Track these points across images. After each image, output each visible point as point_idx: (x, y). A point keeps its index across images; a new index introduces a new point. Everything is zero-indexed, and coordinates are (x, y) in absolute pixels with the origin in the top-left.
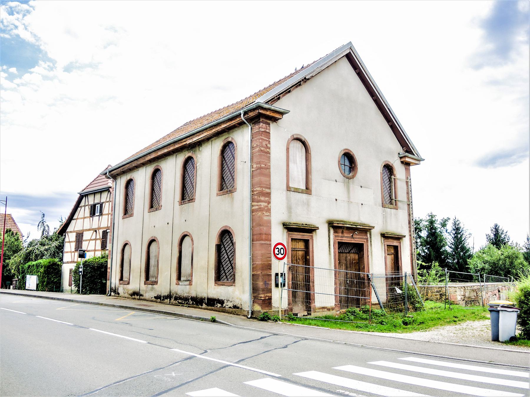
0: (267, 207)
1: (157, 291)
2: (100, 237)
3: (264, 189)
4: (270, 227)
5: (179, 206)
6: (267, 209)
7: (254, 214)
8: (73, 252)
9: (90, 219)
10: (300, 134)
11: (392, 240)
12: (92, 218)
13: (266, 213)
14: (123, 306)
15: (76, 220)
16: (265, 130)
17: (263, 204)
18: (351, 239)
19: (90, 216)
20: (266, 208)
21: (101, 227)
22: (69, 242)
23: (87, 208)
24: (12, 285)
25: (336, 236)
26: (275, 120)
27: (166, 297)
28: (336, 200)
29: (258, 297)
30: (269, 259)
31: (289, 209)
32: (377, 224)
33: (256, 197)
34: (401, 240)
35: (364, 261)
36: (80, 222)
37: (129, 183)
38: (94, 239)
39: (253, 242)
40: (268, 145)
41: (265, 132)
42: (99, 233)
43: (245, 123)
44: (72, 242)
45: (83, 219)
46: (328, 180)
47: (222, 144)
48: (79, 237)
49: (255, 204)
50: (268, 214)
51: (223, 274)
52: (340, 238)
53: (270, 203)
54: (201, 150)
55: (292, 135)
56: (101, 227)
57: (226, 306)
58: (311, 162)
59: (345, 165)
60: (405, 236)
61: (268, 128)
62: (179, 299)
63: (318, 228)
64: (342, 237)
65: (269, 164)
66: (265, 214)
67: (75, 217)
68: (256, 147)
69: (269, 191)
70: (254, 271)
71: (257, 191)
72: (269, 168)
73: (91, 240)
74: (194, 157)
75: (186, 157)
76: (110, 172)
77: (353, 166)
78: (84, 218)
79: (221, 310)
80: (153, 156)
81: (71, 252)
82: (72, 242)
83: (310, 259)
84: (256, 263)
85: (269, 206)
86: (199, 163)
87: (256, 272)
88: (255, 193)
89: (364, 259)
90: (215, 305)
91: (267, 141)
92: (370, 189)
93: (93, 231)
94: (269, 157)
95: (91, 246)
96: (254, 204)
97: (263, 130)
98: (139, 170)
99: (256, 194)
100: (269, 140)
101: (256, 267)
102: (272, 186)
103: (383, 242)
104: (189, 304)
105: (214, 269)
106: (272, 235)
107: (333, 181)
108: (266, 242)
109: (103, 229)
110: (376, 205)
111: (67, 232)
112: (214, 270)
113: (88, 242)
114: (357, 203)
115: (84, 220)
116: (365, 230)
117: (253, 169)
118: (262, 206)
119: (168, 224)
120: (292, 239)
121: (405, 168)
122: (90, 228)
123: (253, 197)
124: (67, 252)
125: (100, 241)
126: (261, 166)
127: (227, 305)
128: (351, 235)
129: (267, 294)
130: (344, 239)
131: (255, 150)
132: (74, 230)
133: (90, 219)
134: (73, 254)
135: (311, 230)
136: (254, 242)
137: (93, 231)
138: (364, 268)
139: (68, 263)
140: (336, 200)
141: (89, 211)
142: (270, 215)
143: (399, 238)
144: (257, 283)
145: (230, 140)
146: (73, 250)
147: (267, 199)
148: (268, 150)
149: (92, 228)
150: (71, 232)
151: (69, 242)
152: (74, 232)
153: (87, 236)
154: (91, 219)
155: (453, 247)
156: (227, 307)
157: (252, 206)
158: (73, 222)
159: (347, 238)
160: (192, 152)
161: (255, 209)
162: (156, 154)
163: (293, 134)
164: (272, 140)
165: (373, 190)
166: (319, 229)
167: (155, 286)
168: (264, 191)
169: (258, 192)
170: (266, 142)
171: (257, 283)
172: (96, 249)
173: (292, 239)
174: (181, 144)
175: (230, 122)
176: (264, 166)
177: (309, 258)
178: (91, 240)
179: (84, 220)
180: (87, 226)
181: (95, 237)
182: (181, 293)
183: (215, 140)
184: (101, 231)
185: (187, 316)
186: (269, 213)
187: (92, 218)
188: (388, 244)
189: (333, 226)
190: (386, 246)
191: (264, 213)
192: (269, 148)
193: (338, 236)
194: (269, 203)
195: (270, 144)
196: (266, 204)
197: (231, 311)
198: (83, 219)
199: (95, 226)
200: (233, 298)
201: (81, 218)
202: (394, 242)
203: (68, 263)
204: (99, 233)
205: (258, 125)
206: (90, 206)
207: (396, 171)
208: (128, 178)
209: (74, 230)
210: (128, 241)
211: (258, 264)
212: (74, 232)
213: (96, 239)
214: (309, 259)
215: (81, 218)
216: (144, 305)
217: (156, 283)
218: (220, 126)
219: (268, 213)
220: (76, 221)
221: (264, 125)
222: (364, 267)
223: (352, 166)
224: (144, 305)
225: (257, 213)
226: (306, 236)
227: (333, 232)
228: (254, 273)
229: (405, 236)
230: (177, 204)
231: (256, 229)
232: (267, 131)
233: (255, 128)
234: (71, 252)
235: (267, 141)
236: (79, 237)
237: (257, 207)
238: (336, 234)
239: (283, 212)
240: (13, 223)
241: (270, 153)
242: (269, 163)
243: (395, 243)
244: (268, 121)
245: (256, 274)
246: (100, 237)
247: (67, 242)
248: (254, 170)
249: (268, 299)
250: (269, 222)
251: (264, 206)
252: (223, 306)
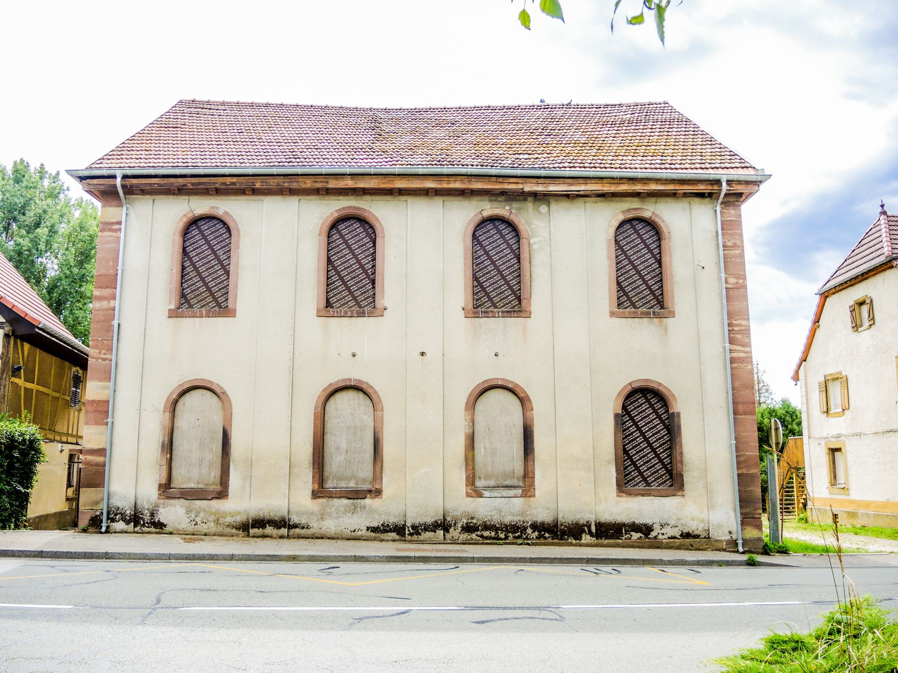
1: (380, 514)
7: (735, 365)
14: (525, 558)
27: (434, 527)
29: (756, 514)
39: (736, 416)
43: (117, 193)
47: (621, 217)
51: (633, 473)
57: (660, 535)
62: (483, 530)
70: (742, 468)
71: (740, 325)
76: (125, 177)
79: (646, 545)
80: (350, 183)
87: (748, 470)
90: (623, 536)
101: (745, 462)
104: (527, 538)
105: (614, 464)
123: (732, 335)
127: (663, 534)
131: (729, 252)
136: (740, 417)
144: (752, 488)
156: (660, 537)
161: (739, 358)
162: (383, 183)
171: (752, 488)
174: (495, 185)
175: (677, 185)
182: (492, 516)
183: (595, 202)
185: (669, 561)
197: (678, 544)
200: (679, 519)
205: (734, 209)
211: (748, 456)
216: (458, 551)
218: (644, 183)
224: (458, 551)
225: (744, 365)
228: (740, 472)
231: (743, 393)
233: (726, 213)
240: (648, 228)
245: (747, 474)
248: (731, 288)
252: (650, 536)
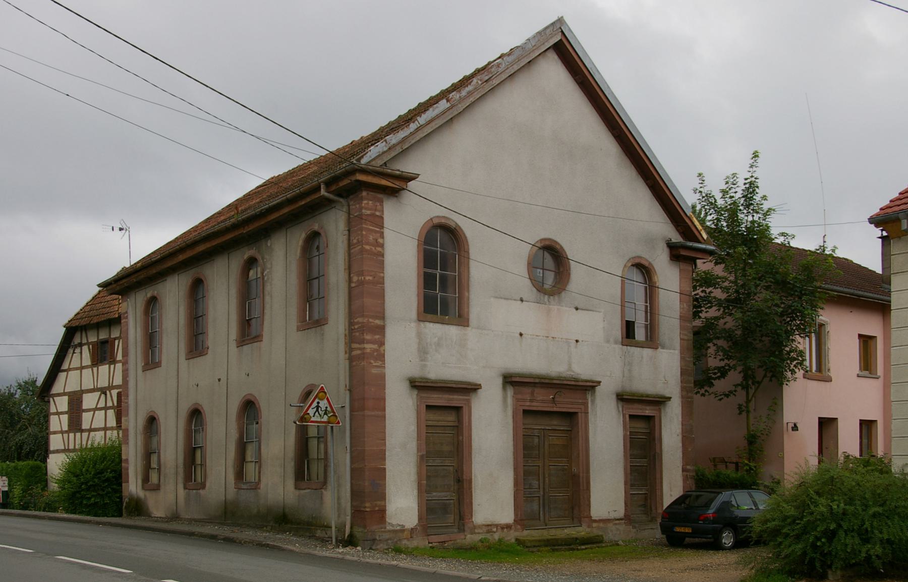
0: (377, 350)
2: (113, 404)
3: (371, 320)
4: (382, 387)
5: (236, 349)
6: (377, 355)
8: (66, 432)
9: (92, 370)
10: (446, 216)
11: (640, 406)
12: (96, 368)
13: (375, 363)
15: (66, 373)
16: (373, 212)
17: (369, 347)
18: (551, 405)
19: (93, 365)
20: (375, 354)
21: (114, 385)
22: (58, 413)
23: (85, 348)
24: (362, 549)
25: (518, 400)
26: (394, 192)
28: (521, 335)
30: (383, 441)
31: (423, 352)
32: (610, 377)
33: (357, 334)
34: (662, 407)
35: (578, 444)
36: (74, 375)
37: (153, 301)
38: (103, 407)
40: (380, 240)
41: (373, 215)
42: (111, 397)
44: (62, 413)
45: (79, 371)
46: (505, 299)
48: (75, 400)
49: (356, 347)
50: (379, 363)
52: (528, 404)
53: (384, 344)
54: (269, 245)
55: (429, 218)
56: (114, 385)
58: (469, 268)
59: (543, 269)
60: (670, 398)
61: (379, 207)
63: (480, 385)
64: (531, 401)
65: (382, 275)
66: (374, 364)
67: (65, 366)
68: (356, 243)
69: (382, 324)
72: (381, 282)
73: (96, 409)
74: (259, 257)
75: (246, 257)
77: (561, 270)
78: (82, 368)
81: (62, 432)
82: (62, 413)
83: (464, 440)
84: (358, 448)
85: (382, 349)
86: (268, 270)
88: (356, 327)
89: (579, 441)
91: (376, 232)
92: (596, 311)
93: (99, 393)
94: (382, 262)
95: (99, 419)
96: (354, 346)
97: (369, 212)
98: (167, 281)
99: (358, 328)
100: (382, 230)
102: (389, 312)
103: (621, 409)
106: (386, 400)
107: (515, 300)
108: (376, 413)
109: (117, 389)
110: (608, 341)
111: (52, 394)
112: (207, 465)
113: (92, 412)
114: (566, 339)
115: (81, 372)
116: (587, 388)
117: (353, 285)
118: (368, 351)
119: (219, 380)
120: (427, 406)
121: (680, 269)
122: (94, 387)
124: (55, 433)
125: (114, 411)
126: (364, 278)
128: (551, 397)
129: (376, 502)
130: (534, 404)
132: (64, 390)
133: (92, 370)
134: (66, 435)
135: (470, 389)
136: (356, 413)
137: (99, 393)
138: (579, 457)
139: (57, 451)
140: (521, 335)
141: (90, 353)
142: (383, 365)
143: (660, 401)
145: (316, 227)
146: (65, 428)
147: (377, 337)
148: (379, 249)
149: (97, 386)
150: (59, 395)
151: (58, 413)
152: (64, 394)
153: (89, 401)
154: (95, 369)
155: (89, 446)
157: (351, 350)
158: (62, 376)
159: (542, 400)
160: (254, 249)
163: (432, 217)
164: (387, 232)
165: (602, 313)
166: (481, 388)
167: (201, 491)
168: (372, 324)
169: (360, 325)
170: (374, 234)
172: (107, 426)
173: (427, 406)
176: (371, 278)
177: (463, 438)
178: (96, 409)
179: (81, 372)
180: (88, 384)
181: (104, 403)
184: (115, 393)
186: (382, 361)
187: (96, 368)
188: (631, 414)
189: (511, 381)
190: (627, 416)
191: (372, 361)
192: (382, 246)
193: (524, 400)
194: (382, 343)
195: (383, 238)
196: (375, 346)
198: (79, 371)
199: (103, 383)
201: (76, 369)
202: (646, 410)
203: (57, 451)
204: (111, 397)
206: (91, 346)
207: (656, 274)
208: (149, 295)
209: (64, 390)
210: (155, 413)
212: (64, 394)
213: (106, 408)
214: (463, 441)
215: (76, 369)
217: (203, 486)
219: (381, 363)
220: (67, 374)
221: (370, 202)
222: (579, 454)
223: (559, 269)
226: (455, 400)
227: (512, 393)
229: (670, 398)
230: (233, 345)
232: (378, 213)
234: (62, 432)
235: (376, 232)
236: (75, 400)
237: (358, 352)
238: (520, 396)
239: (410, 359)
241: (383, 256)
242: (381, 273)
243: (647, 412)
244: (380, 196)
246: (113, 404)
247: (54, 413)
249: (378, 510)
250: (382, 377)
251: (372, 349)
